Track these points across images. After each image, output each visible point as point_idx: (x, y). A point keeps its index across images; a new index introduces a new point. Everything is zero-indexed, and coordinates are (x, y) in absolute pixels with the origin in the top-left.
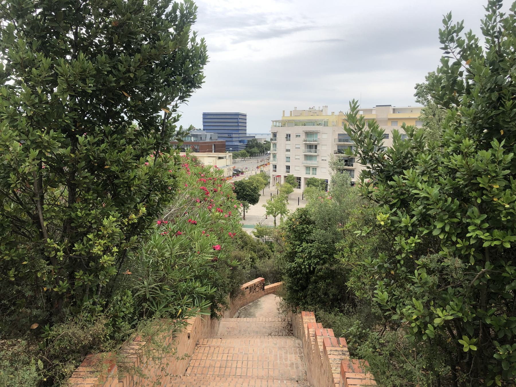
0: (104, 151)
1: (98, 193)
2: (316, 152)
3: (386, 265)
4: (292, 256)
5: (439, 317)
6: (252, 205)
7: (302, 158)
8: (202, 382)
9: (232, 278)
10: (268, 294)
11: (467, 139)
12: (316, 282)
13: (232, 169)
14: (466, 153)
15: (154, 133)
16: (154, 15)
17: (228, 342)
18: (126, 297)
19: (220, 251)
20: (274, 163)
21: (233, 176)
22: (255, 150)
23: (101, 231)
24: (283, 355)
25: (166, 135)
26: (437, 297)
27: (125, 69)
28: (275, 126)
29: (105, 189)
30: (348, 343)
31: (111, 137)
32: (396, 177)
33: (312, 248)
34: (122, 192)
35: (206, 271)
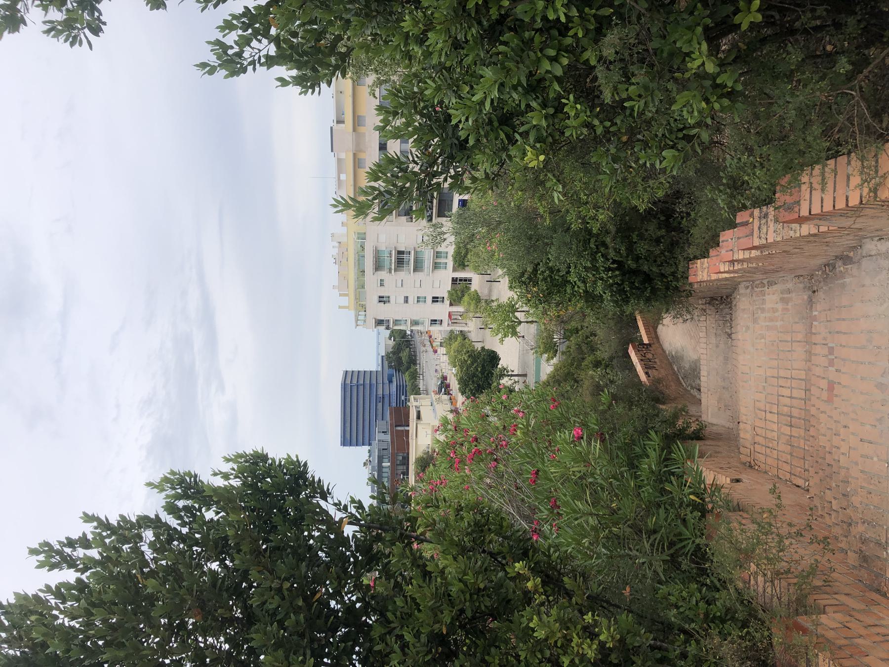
0: (417, 635)
1: (490, 646)
2: (409, 253)
3: (613, 151)
4: (591, 298)
5: (703, 64)
6: (501, 362)
7: (420, 275)
8: (820, 460)
9: (631, 403)
10: (657, 337)
11: (402, 24)
12: (637, 259)
13: (438, 396)
14: (425, 25)
15: (383, 544)
16: (182, 546)
17: (746, 411)
18: (671, 597)
19: (584, 425)
20: (427, 323)
21: (449, 394)
22: (404, 355)
23: (556, 642)
24: (768, 315)
25: (387, 523)
26: (668, 67)
27: (276, 597)
28: (365, 321)
29: (482, 632)
30: (745, 207)
31: (393, 622)
32: (462, 134)
33: (579, 266)
34: (488, 604)
35: (619, 448)
